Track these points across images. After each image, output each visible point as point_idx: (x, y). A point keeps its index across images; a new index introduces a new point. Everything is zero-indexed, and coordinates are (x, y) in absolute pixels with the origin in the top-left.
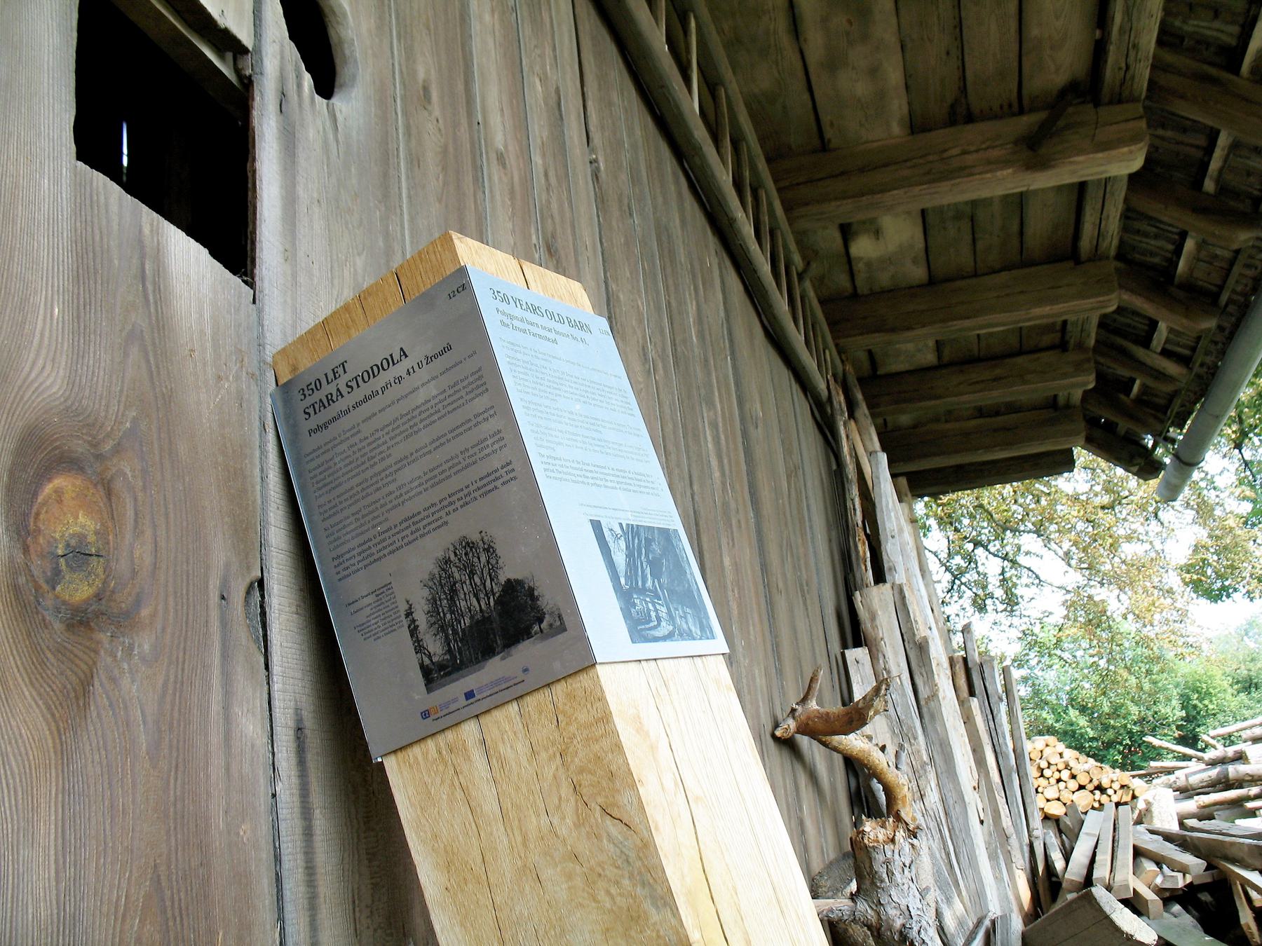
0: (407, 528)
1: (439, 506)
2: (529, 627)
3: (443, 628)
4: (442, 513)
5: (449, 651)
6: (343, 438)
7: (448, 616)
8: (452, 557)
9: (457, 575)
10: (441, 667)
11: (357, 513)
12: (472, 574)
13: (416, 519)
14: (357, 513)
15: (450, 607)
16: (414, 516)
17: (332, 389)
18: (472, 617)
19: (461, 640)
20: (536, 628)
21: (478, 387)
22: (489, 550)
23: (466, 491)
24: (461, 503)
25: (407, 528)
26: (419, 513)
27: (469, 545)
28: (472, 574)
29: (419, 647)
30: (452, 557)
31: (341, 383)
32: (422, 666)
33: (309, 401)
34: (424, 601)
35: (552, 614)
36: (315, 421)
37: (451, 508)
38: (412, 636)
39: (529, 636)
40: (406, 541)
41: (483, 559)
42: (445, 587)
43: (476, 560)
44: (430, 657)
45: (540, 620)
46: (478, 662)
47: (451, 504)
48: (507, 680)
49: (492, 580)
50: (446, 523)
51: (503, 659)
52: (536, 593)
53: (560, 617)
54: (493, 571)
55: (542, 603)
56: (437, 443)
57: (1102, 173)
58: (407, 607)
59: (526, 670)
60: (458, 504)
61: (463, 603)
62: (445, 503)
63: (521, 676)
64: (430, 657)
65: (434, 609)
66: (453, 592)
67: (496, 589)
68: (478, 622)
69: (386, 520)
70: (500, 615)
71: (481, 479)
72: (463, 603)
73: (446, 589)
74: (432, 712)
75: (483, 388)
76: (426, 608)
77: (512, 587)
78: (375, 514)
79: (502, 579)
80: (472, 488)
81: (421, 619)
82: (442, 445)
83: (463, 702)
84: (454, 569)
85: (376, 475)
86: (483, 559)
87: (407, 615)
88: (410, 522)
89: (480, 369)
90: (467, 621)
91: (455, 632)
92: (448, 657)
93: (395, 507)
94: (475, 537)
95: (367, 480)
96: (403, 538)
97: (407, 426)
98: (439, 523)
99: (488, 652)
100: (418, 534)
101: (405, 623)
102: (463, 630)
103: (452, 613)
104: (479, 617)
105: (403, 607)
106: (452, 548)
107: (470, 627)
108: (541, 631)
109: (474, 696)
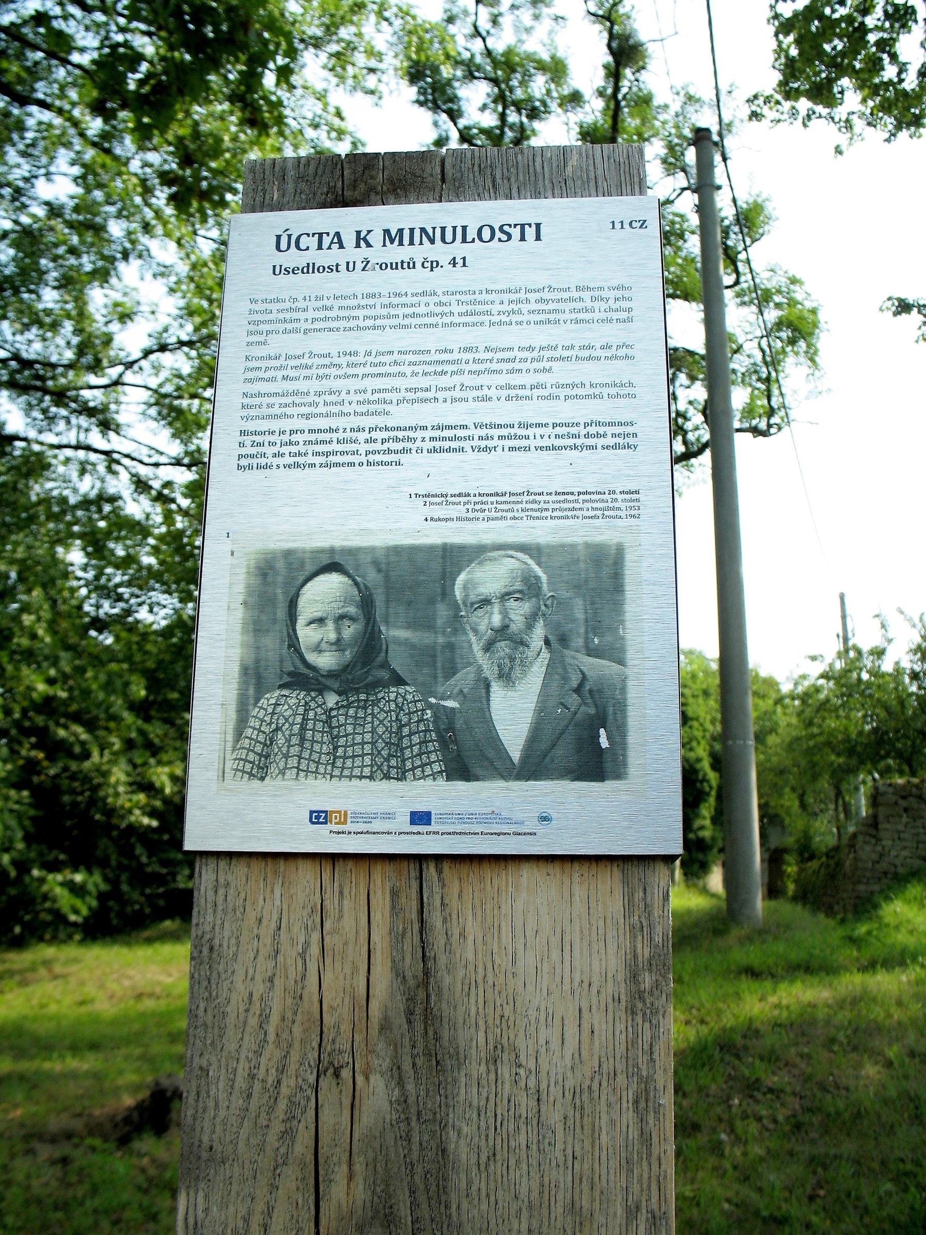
48: (508, 821)
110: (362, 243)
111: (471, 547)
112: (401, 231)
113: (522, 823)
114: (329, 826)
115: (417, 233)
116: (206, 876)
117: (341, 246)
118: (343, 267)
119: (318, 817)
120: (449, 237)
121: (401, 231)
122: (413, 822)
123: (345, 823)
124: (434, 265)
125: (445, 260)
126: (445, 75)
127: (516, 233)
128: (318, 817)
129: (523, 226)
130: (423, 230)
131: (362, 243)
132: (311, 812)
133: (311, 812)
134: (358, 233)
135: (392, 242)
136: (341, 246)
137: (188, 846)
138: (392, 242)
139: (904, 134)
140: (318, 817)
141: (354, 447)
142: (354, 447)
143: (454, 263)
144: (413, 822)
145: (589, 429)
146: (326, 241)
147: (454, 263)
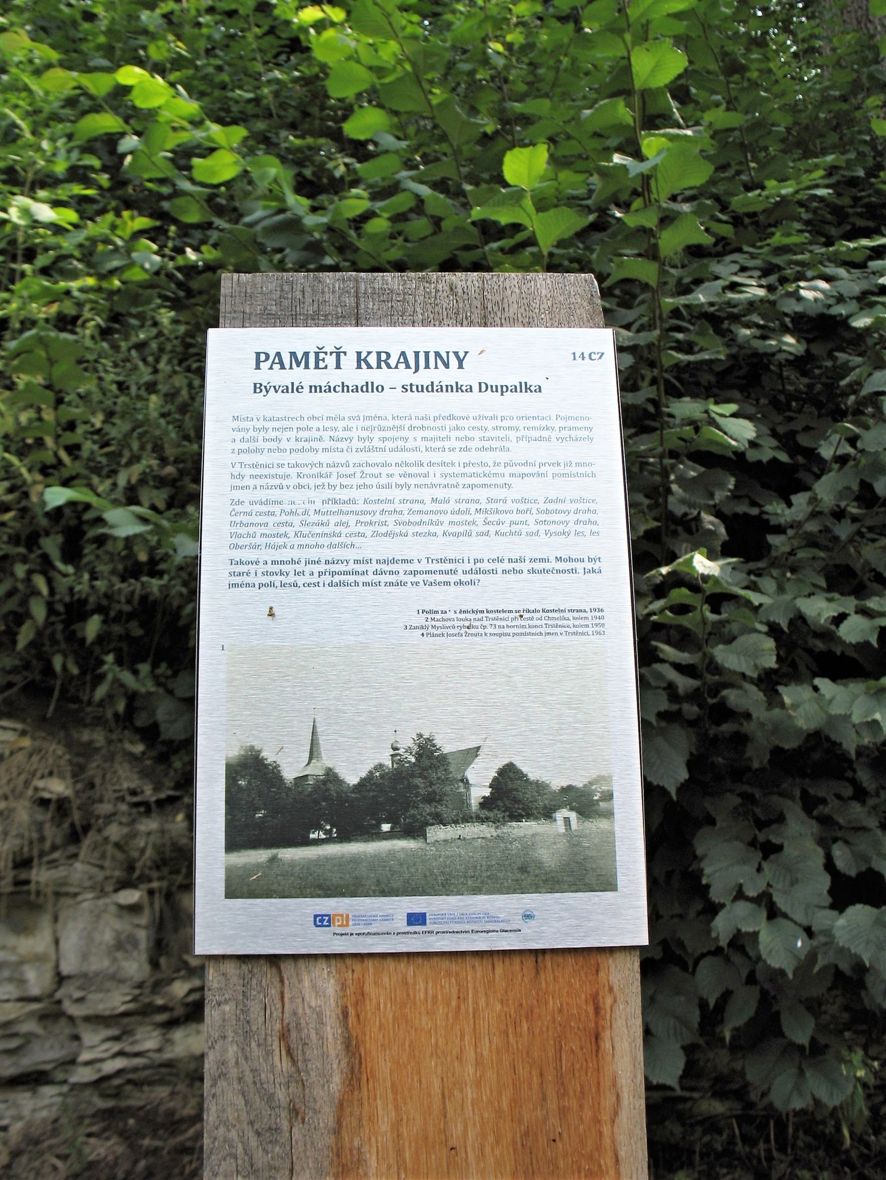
109: (424, 923)
110: (363, 364)
111: (193, 685)
112: (306, 354)
113: (508, 921)
114: (332, 929)
115: (432, 357)
116: (211, 974)
118: (476, 388)
119: (322, 920)
120: (393, 362)
121: (306, 354)
122: (410, 923)
126: (106, 176)
128: (322, 921)
130: (437, 354)
131: (363, 364)
132: (316, 916)
133: (316, 916)
134: (359, 354)
135: (298, 365)
137: (199, 950)
138: (298, 365)
144: (410, 923)
145: (479, 565)
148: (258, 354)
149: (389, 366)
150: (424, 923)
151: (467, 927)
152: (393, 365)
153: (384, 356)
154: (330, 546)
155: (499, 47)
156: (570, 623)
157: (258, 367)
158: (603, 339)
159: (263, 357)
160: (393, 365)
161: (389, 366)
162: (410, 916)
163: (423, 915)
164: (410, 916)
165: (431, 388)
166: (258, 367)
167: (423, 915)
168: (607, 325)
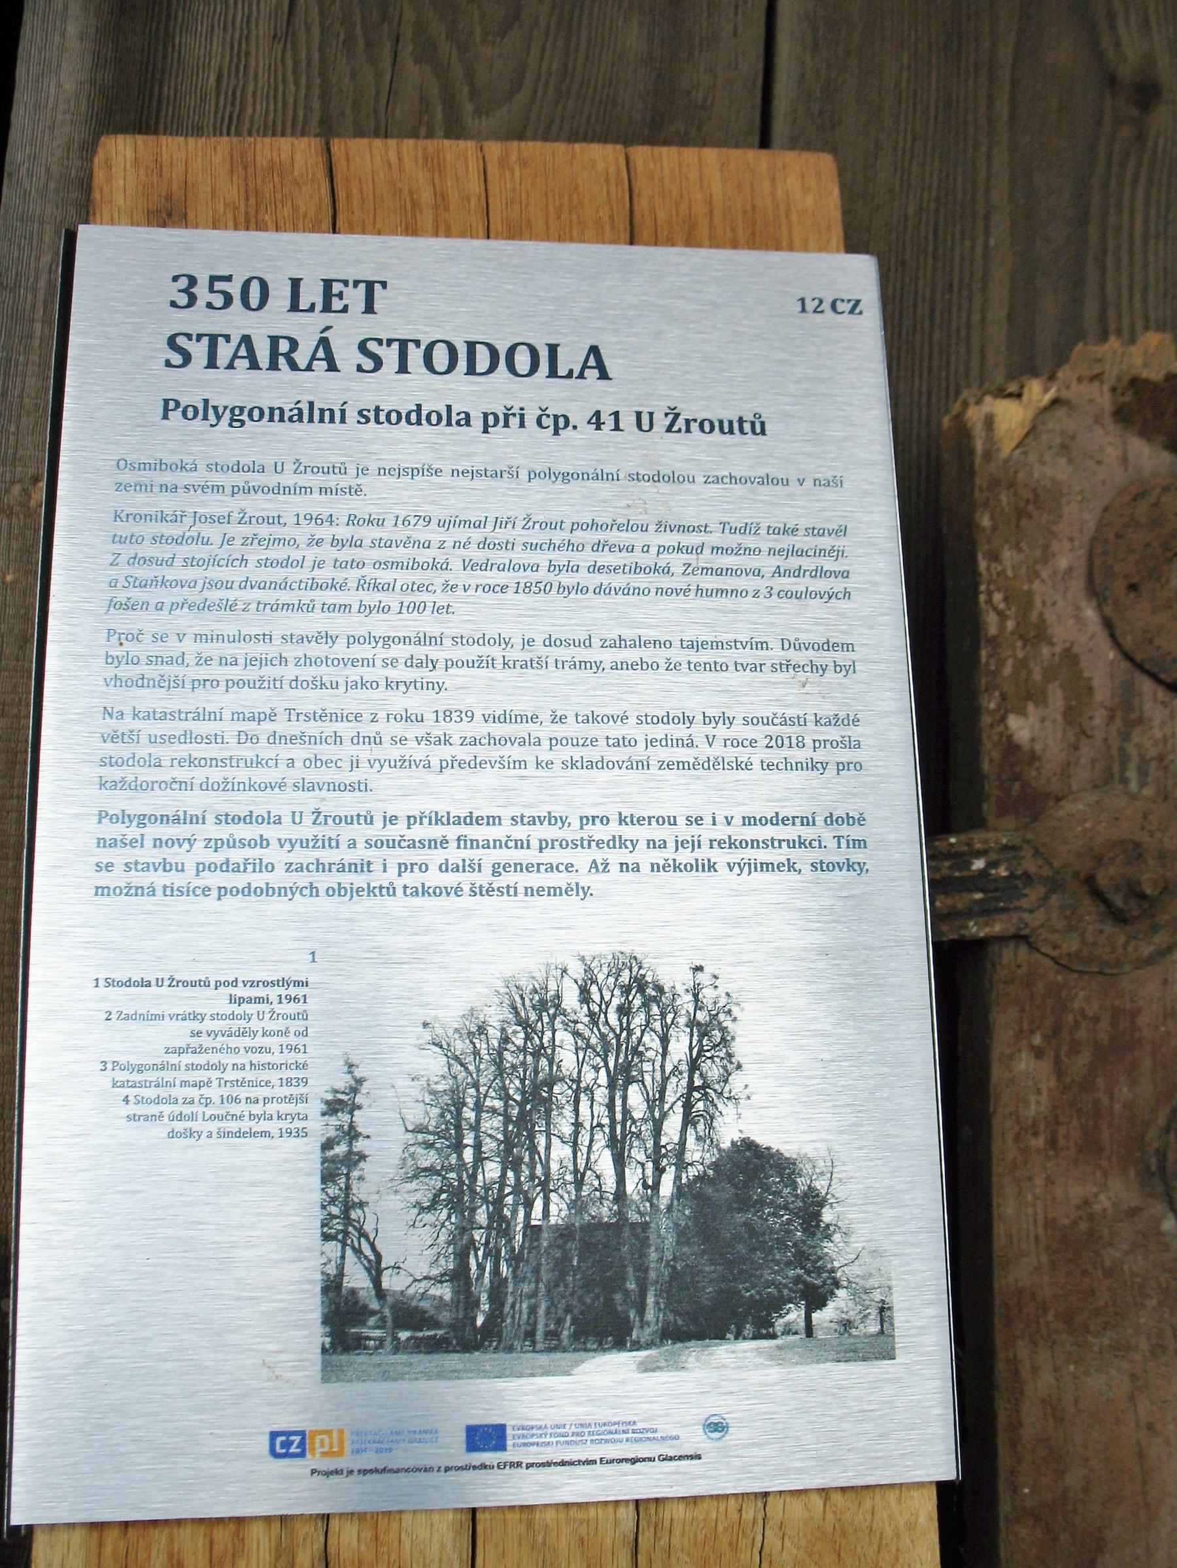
0: (432, 844)
1: (573, 832)
2: (777, 1305)
3: (457, 1197)
4: (582, 858)
5: (459, 1276)
6: (288, 479)
7: (492, 1170)
8: (571, 1000)
9: (568, 1059)
10: (408, 1315)
11: (258, 718)
12: (621, 1078)
13: (473, 832)
14: (258, 718)
15: (508, 1143)
16: (471, 820)
17: (306, 329)
18: (578, 1206)
19: (515, 1259)
20: (795, 1315)
21: (819, 573)
22: (711, 1032)
23: (685, 831)
24: (658, 856)
25: (432, 844)
26: (494, 820)
27: (641, 989)
28: (621, 1078)
29: (343, 1222)
30: (571, 1000)
31: (346, 334)
32: (332, 1286)
33: (199, 320)
34: (415, 1090)
35: (859, 1294)
36: (301, 1108)
37: (615, 857)
38: (328, 1177)
39: (764, 1331)
40: (412, 879)
41: (680, 1048)
42: (509, 1081)
43: (652, 1041)
44: (375, 1270)
45: (816, 1299)
46: (553, 1342)
47: (617, 842)
48: (646, 1435)
49: (688, 1120)
50: (584, 892)
51: (646, 1367)
52: (827, 1216)
53: (884, 1310)
54: (701, 1098)
55: (837, 1252)
56: (631, 655)
57: (287, 1466)
58: (343, 1081)
59: (717, 1427)
60: (645, 857)
61: (560, 1152)
62: (599, 832)
63: (695, 1439)
64: (375, 1270)
65: (450, 1127)
66: (537, 1099)
67: (694, 1152)
68: (598, 1225)
69: (361, 787)
70: (683, 1236)
71: (748, 821)
72: (560, 1152)
73: (514, 1085)
74: (319, 1444)
75: (838, 585)
76: (415, 1115)
77: (752, 1164)
78: (327, 751)
79: (728, 1132)
80: (707, 832)
81: (386, 1138)
82: (643, 665)
83: (454, 1448)
84: (563, 1036)
85: (369, 639)
86: (680, 1048)
87: (333, 1107)
88: (452, 832)
89: (842, 531)
90: (559, 1210)
91: (500, 1224)
92: (445, 1292)
93: (404, 763)
94: (672, 974)
95: (331, 639)
96: (402, 868)
97: (541, 558)
98: (559, 879)
99: (604, 1329)
100: (465, 879)
101: (319, 1127)
102: (532, 1232)
103: (511, 1162)
104: (605, 1211)
105: (326, 1080)
106: (577, 970)
107: (564, 1233)
108: (809, 1330)
109: (502, 1447)
117: (332, 367)
120: (301, 358)
122: (472, 1447)
123: (340, 1453)
124: (561, 423)
125: (579, 414)
127: (390, 355)
128: (287, 1444)
129: (403, 344)
132: (274, 1435)
133: (274, 1435)
136: (332, 367)
139: (367, 1153)
140: (287, 1444)
141: (751, 562)
142: (751, 562)
143: (597, 420)
144: (472, 1447)
146: (225, 352)
147: (597, 420)
148: (166, 401)
149: (294, 366)
150: (502, 1447)
151: (595, 1452)
152: (302, 362)
153: (284, 346)
154: (206, 786)
155: (496, 1174)
156: (584, 558)
157: (165, 417)
158: (859, 275)
159: (172, 405)
160: (302, 362)
161: (294, 366)
162: (472, 1431)
163: (500, 1430)
164: (472, 1431)
165: (417, 416)
166: (165, 417)
167: (500, 1430)
168: (852, 246)
